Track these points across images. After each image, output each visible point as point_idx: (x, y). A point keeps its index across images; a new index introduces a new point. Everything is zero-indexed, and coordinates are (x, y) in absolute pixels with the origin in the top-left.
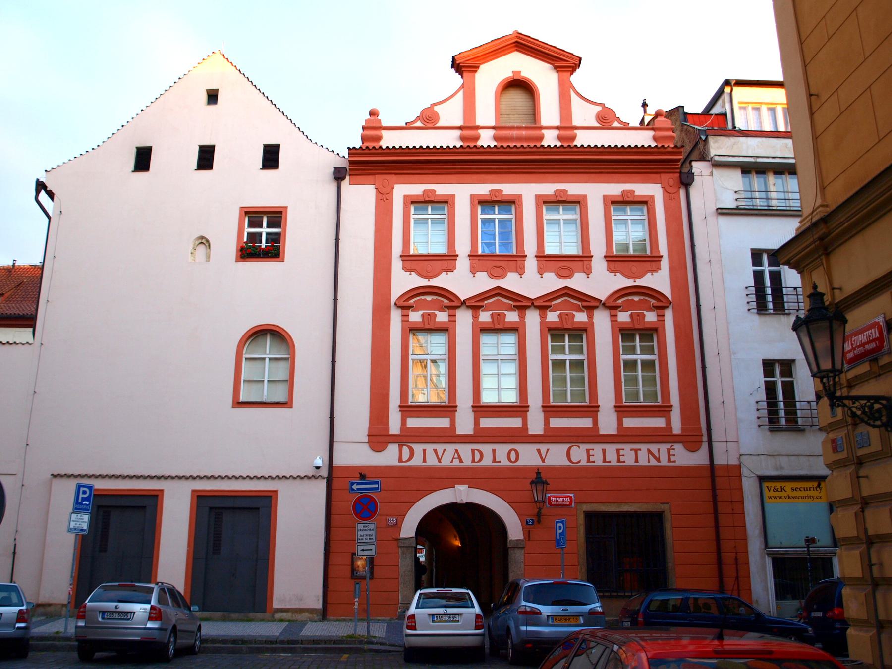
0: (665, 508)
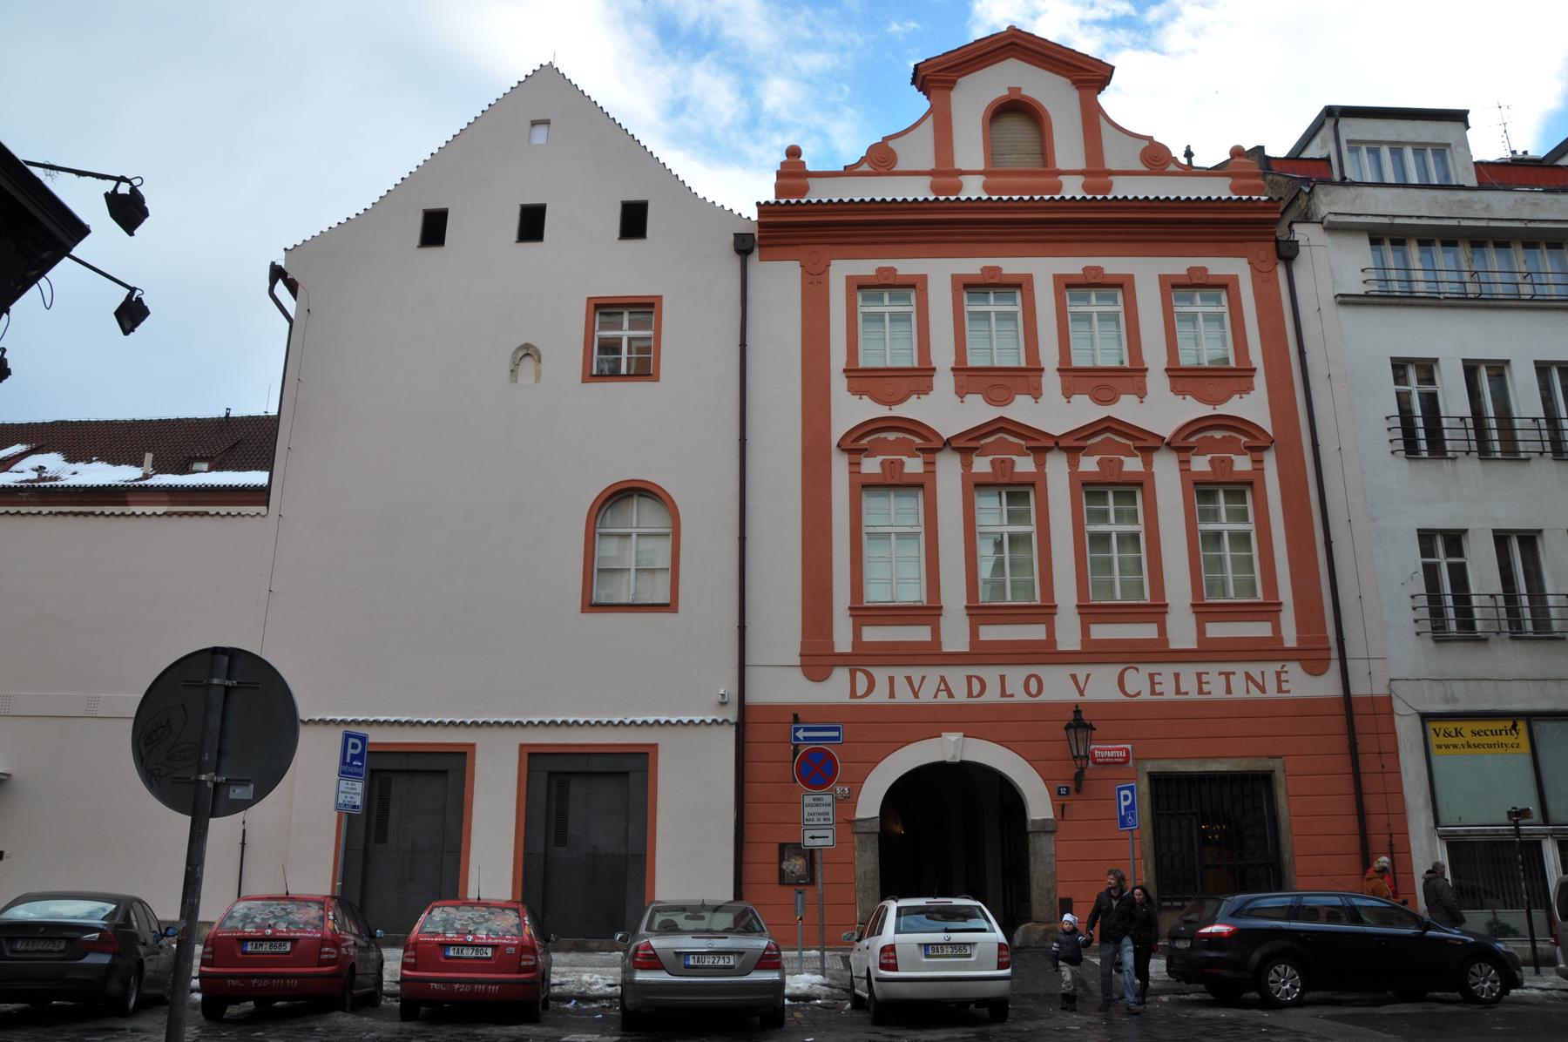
0: (1275, 764)
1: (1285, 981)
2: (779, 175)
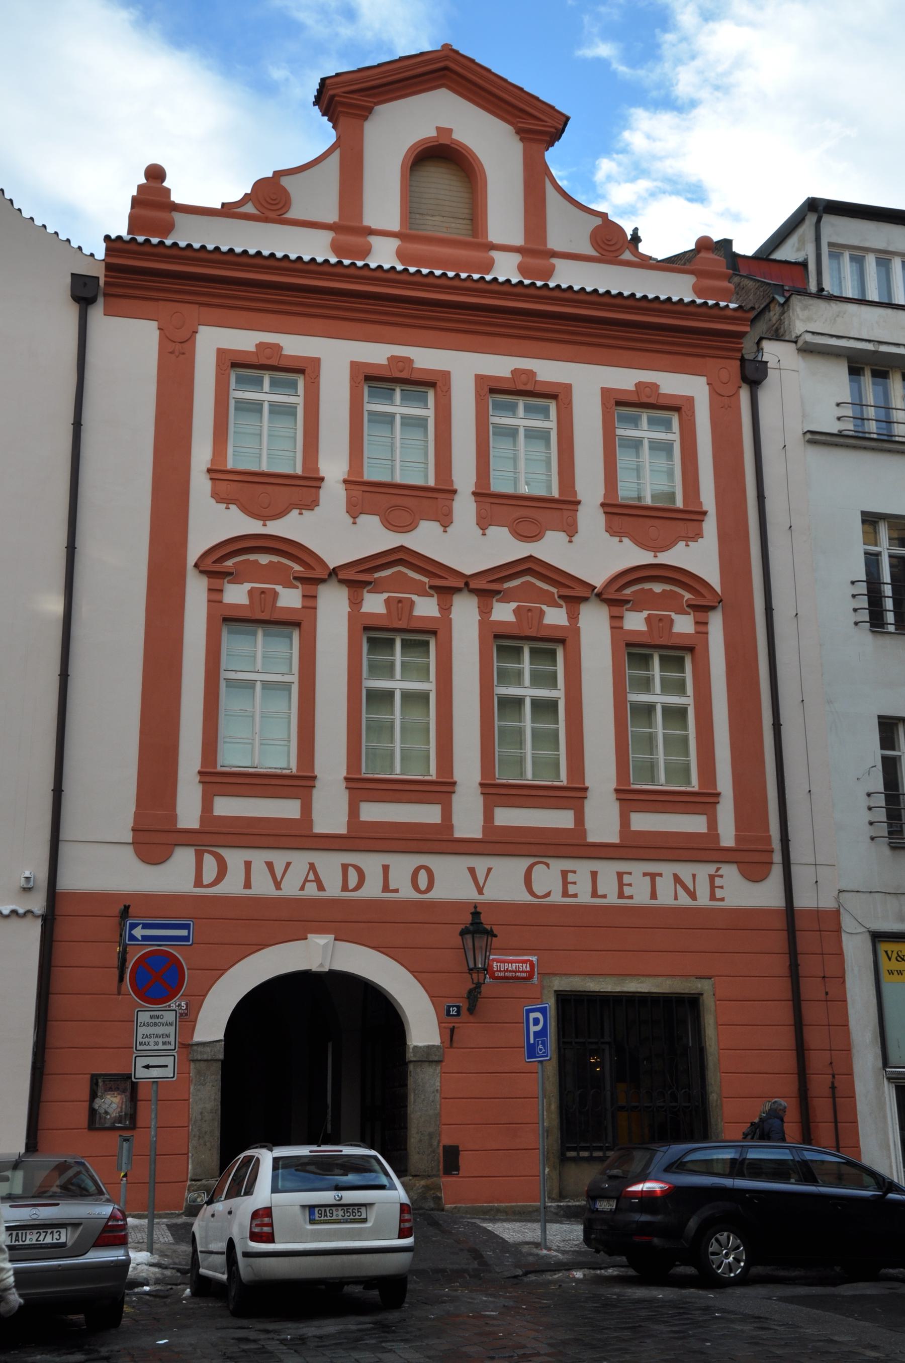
0: (704, 986)
1: (728, 1254)
2: (135, 202)
